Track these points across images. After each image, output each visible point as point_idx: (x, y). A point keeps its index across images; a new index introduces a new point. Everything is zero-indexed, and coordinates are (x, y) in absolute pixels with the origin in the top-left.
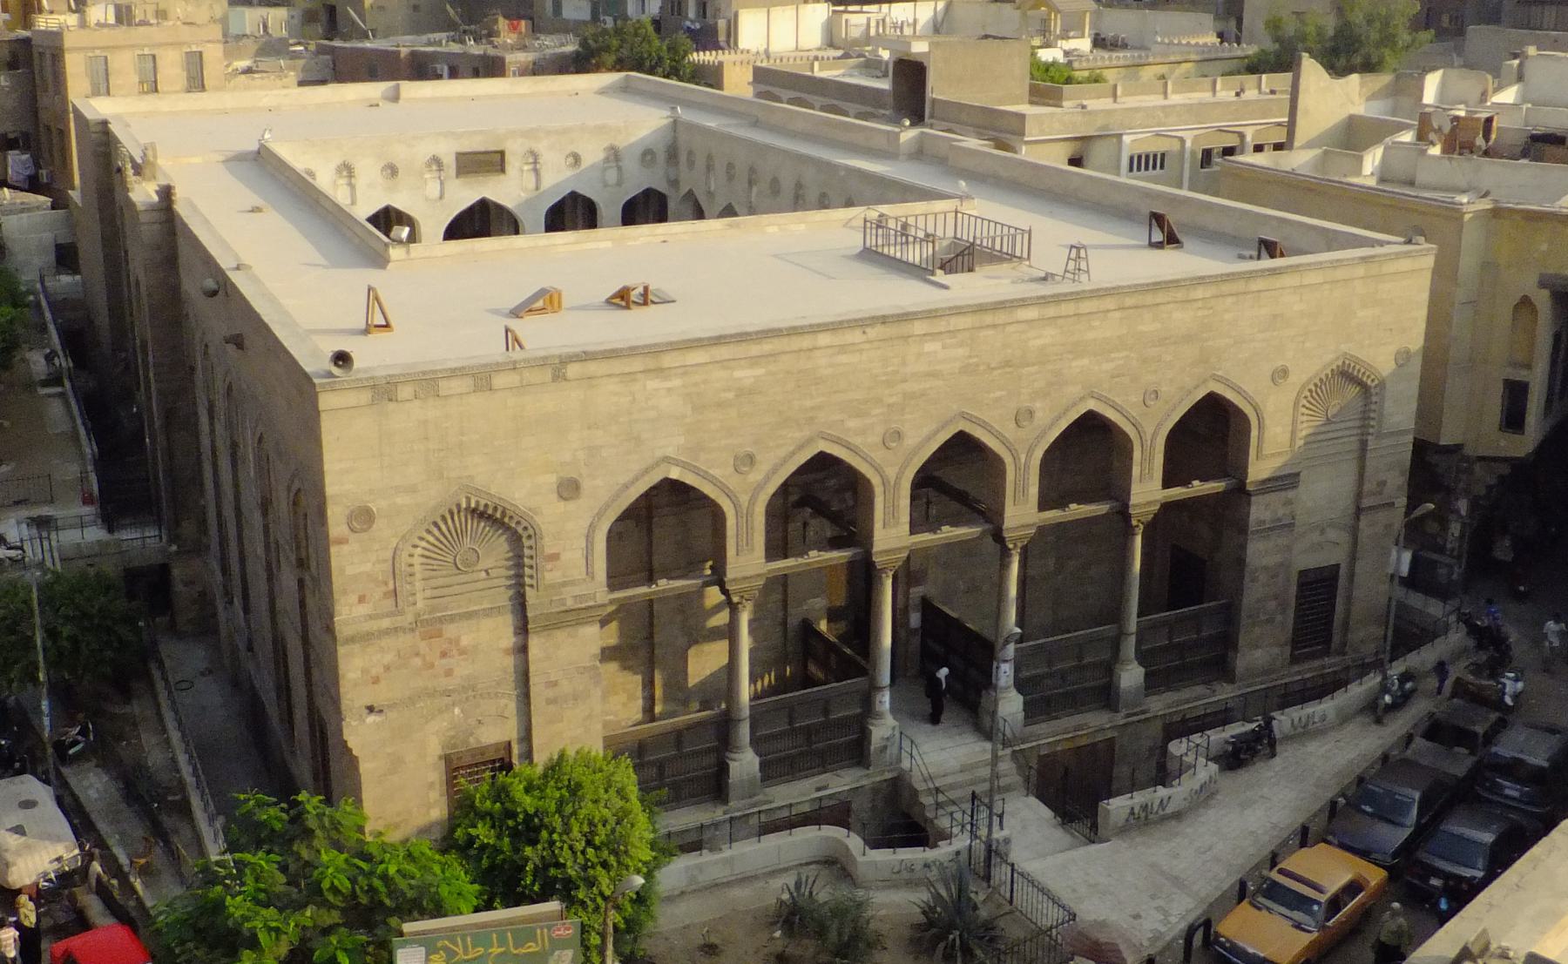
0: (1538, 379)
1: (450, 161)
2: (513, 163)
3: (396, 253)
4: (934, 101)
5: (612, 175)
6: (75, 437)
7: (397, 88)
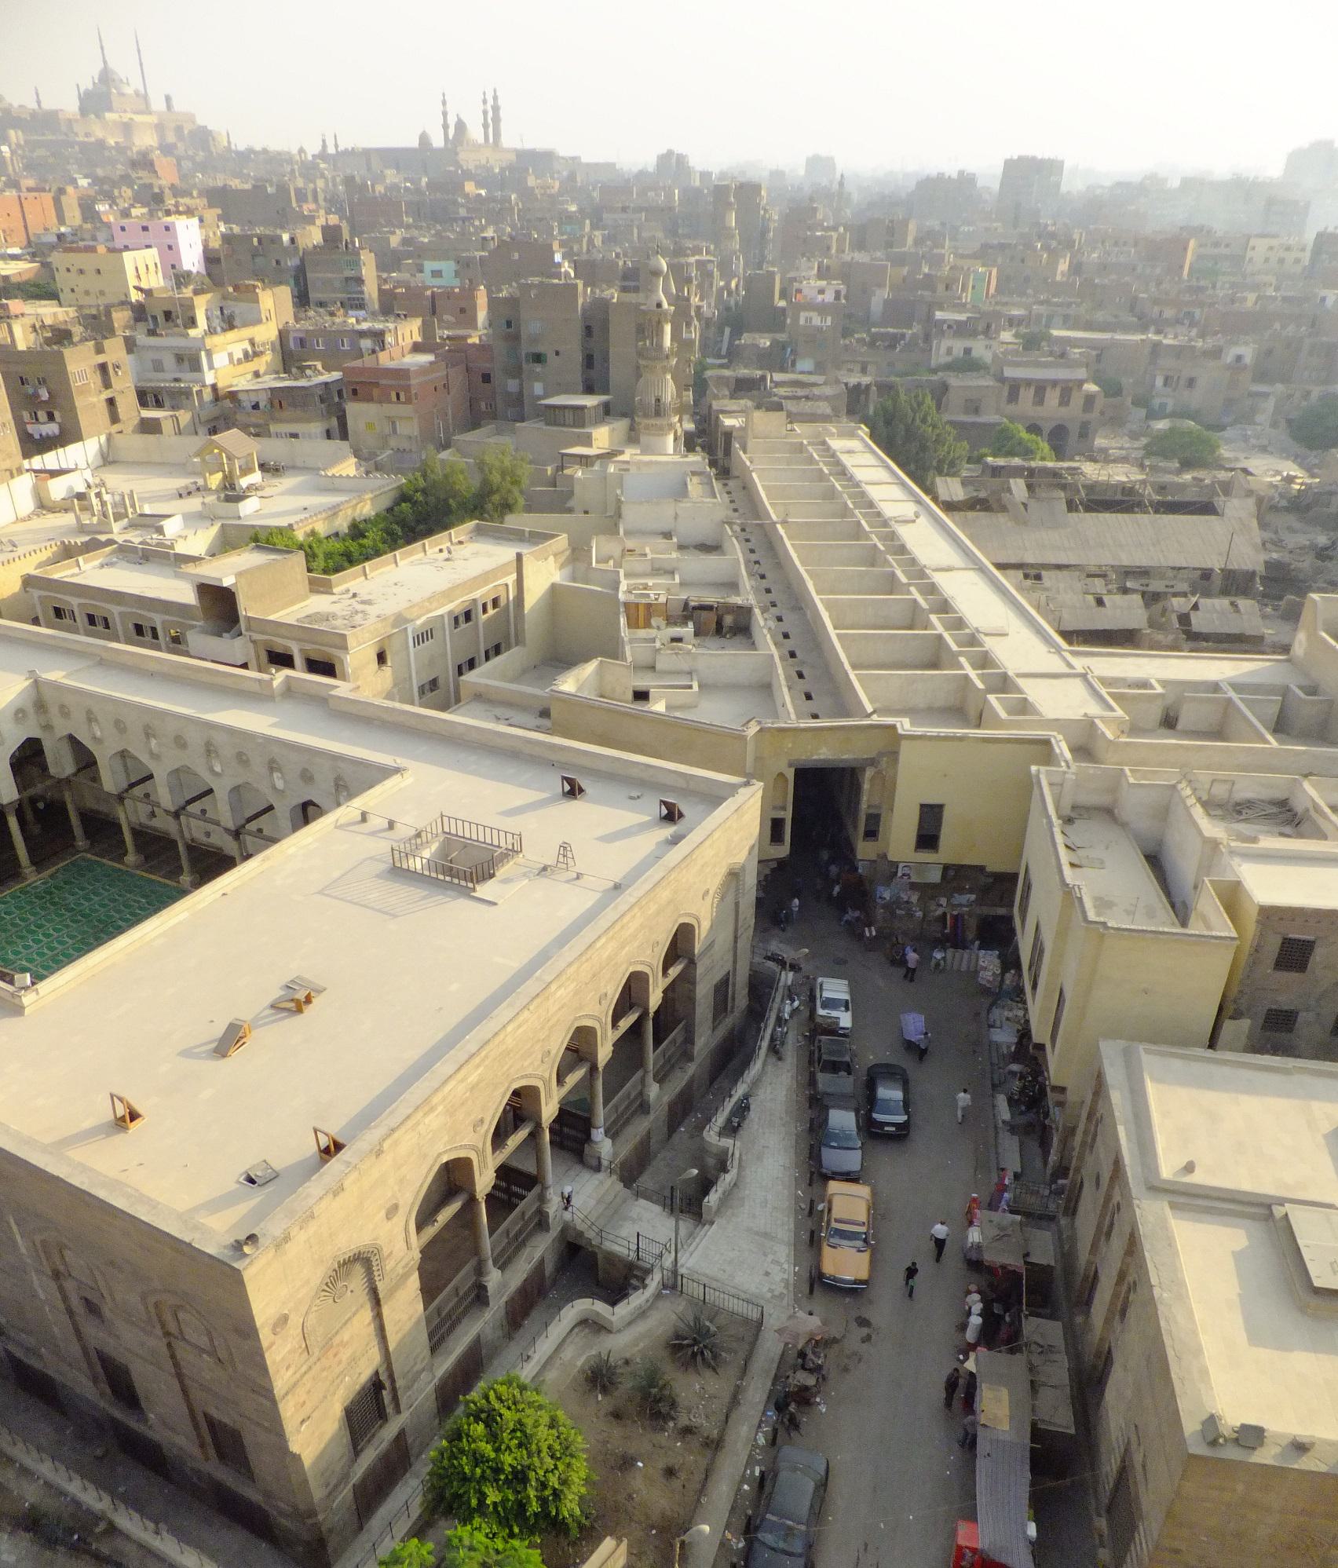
0: (788, 815)
3: (28, 999)
4: (249, 619)
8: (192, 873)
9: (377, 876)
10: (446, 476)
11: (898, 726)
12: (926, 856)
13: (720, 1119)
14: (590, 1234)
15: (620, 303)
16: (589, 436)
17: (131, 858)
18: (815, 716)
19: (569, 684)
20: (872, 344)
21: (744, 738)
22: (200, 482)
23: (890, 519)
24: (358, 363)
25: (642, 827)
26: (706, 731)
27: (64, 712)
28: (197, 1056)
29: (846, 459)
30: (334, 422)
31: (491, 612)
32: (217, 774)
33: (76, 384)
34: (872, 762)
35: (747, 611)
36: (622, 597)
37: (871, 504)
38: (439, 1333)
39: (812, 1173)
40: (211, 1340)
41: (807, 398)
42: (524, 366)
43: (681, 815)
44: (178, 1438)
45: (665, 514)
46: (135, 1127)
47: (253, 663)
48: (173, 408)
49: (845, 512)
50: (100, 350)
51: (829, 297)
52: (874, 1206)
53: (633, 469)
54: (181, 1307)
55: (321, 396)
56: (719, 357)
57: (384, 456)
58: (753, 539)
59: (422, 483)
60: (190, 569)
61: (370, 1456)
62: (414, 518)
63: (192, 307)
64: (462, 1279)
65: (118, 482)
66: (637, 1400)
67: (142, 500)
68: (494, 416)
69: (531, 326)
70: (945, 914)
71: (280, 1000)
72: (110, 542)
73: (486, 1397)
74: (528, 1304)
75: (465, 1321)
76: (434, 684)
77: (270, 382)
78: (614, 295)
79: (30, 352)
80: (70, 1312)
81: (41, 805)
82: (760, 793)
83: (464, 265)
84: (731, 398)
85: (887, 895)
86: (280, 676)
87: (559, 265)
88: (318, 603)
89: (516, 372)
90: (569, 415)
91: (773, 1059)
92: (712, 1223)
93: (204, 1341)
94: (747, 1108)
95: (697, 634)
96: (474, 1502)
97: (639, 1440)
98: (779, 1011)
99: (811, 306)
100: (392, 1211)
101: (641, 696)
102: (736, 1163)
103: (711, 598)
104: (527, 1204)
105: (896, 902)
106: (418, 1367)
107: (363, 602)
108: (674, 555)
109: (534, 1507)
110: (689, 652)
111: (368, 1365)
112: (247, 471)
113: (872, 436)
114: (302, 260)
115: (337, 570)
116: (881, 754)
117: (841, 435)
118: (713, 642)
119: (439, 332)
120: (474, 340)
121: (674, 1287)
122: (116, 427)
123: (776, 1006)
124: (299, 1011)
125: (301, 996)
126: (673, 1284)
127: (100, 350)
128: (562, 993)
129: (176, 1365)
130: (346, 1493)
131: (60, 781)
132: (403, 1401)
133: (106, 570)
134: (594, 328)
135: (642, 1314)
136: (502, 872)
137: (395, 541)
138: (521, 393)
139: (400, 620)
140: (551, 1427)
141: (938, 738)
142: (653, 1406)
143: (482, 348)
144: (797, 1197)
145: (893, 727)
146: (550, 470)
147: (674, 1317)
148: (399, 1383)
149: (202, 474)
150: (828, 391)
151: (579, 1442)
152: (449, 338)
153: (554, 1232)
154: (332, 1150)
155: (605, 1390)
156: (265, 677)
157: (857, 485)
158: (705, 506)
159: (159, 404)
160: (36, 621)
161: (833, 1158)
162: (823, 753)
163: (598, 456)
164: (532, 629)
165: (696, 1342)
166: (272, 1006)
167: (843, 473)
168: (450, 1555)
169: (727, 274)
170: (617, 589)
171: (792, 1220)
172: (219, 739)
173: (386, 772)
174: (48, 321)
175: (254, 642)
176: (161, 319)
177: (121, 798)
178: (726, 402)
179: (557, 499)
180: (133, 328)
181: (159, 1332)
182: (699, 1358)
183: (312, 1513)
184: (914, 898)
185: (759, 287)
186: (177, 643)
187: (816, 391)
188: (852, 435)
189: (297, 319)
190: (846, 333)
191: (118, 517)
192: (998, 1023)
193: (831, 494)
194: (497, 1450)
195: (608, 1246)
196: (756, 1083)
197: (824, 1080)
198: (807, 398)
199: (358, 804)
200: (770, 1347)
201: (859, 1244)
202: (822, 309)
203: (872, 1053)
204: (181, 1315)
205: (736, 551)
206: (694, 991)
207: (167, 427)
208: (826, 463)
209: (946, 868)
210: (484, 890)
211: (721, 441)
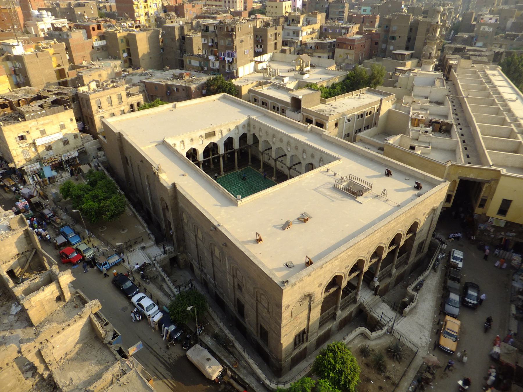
0: (454, 194)
1: (204, 135)
2: (217, 133)
3: (239, 202)
4: (303, 108)
5: (237, 132)
6: (135, 216)
7: (175, 104)
8: (276, 177)
9: (330, 188)
10: (361, 73)
11: (501, 171)
12: (500, 217)
13: (414, 285)
14: (368, 309)
15: (422, 22)
16: (405, 64)
17: (261, 170)
18: (469, 163)
19: (391, 141)
20: (506, 38)
21: (445, 167)
22: (294, 68)
23: (506, 99)
24: (341, 37)
25: (408, 189)
26: (434, 163)
27: (254, 127)
28: (277, 228)
29: (492, 78)
30: (331, 54)
31: (369, 115)
32: (289, 151)
33: (269, 38)
34: (488, 182)
35: (451, 125)
36: (410, 116)
37: (499, 94)
38: (323, 322)
39: (441, 311)
40: (268, 305)
41: (479, 55)
42: (389, 40)
43: (421, 188)
44: (252, 329)
45: (427, 91)
46: (260, 243)
47: (302, 121)
48: (290, 46)
49: (489, 95)
50: (276, 29)
51: (493, 21)
52: (461, 327)
53: (418, 75)
54: (263, 294)
55: (329, 46)
56: (448, 40)
57: (343, 65)
58: (455, 102)
59: (353, 74)
60: (291, 92)
61: (297, 351)
62: (350, 85)
63: (300, 18)
64: (331, 310)
65: (274, 66)
66: (376, 363)
67: (280, 72)
68: (376, 55)
69: (394, 28)
70: (502, 238)
71: (300, 218)
72: (271, 82)
73: (334, 346)
74: (347, 324)
75: (328, 322)
76: (348, 135)
77: (316, 41)
78: (420, 18)
79: (259, 28)
80: (234, 287)
81: (243, 151)
82: (448, 185)
83: (374, 8)
84: (452, 54)
85: (482, 227)
86: (310, 126)
87: (403, 9)
88: (322, 107)
89: (386, 42)
90: (400, 57)
91: (433, 271)
92: (405, 317)
93: (266, 305)
94: (422, 284)
95: (432, 131)
96: (326, 374)
97: (373, 375)
98: (438, 256)
99: (486, 24)
100: (320, 285)
101: (412, 148)
102: (416, 301)
103: (439, 120)
104: (352, 294)
105: (485, 230)
106: (315, 331)
107: (334, 108)
108: (428, 104)
109: (343, 383)
110: (430, 136)
111: (303, 326)
112: (307, 66)
113: (502, 70)
114: (329, 5)
115: (327, 98)
116: (492, 180)
117: (491, 69)
118: (437, 134)
119: (364, 29)
120: (374, 31)
121: (391, 332)
122: (276, 51)
123: (437, 254)
124: (305, 222)
125: (306, 218)
126: (391, 331)
127: (276, 29)
128: (378, 234)
129: (257, 309)
130: (290, 359)
131: (249, 146)
132: (309, 339)
133: (269, 90)
134: (413, 29)
135: (379, 337)
136: (365, 194)
137: (343, 91)
138: (385, 49)
139: (344, 114)
140: (351, 361)
141: (516, 177)
142: (378, 366)
143: (376, 34)
144: (434, 317)
145: (499, 171)
146: (391, 74)
147: (389, 341)
148: (309, 334)
149: (295, 66)
150: (487, 53)
151: (359, 369)
152: (367, 30)
153: (357, 305)
154: (309, 263)
155: (365, 357)
156: (306, 126)
157: (495, 86)
158: (440, 90)
159: (286, 45)
160: (249, 101)
161: (449, 308)
162: (471, 176)
163: (407, 70)
164: (380, 122)
165: (395, 352)
166: (298, 219)
167: (490, 82)
168: (318, 387)
169: (456, 13)
170: (409, 113)
171: (431, 324)
172: (292, 141)
173: (335, 159)
174: (265, 20)
175: (303, 115)
176: (291, 21)
177: (262, 153)
178: (450, 55)
179: (392, 83)
180: (284, 23)
181: (255, 299)
182: (395, 357)
183: (281, 361)
184: (492, 230)
185: (467, 17)
186: (283, 112)
187: (483, 53)
188: (495, 69)
189: (326, 23)
190: (497, 34)
191: (273, 76)
192: (516, 280)
193: (485, 89)
194: (335, 362)
195: (372, 313)
196: (426, 277)
197: (450, 283)
198: (479, 55)
199: (327, 166)
200: (418, 362)
201: (454, 339)
202: (490, 25)
203: (466, 278)
204: (262, 296)
205: (449, 106)
206: (413, 243)
207: (288, 52)
208: (484, 78)
209: (507, 222)
210: (359, 199)
211: (447, 68)
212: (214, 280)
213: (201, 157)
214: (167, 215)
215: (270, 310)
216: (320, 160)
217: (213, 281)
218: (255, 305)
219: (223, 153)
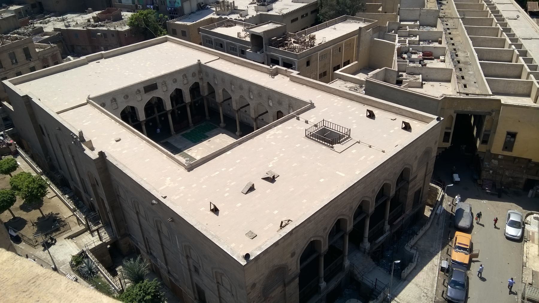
0: (452, 131)
14: (359, 276)
34: (490, 114)
47: (266, 62)
80: (190, 270)
81: (197, 105)
93: (228, 287)
100: (293, 255)
116: (492, 111)
129: (219, 293)
172: (253, 88)
175: (267, 55)
181: (215, 281)
204: (223, 277)
212: (167, 264)
213: (142, 116)
214: (99, 191)
215: (234, 293)
216: (289, 106)
217: (165, 267)
218: (216, 288)
219: (190, 101)
